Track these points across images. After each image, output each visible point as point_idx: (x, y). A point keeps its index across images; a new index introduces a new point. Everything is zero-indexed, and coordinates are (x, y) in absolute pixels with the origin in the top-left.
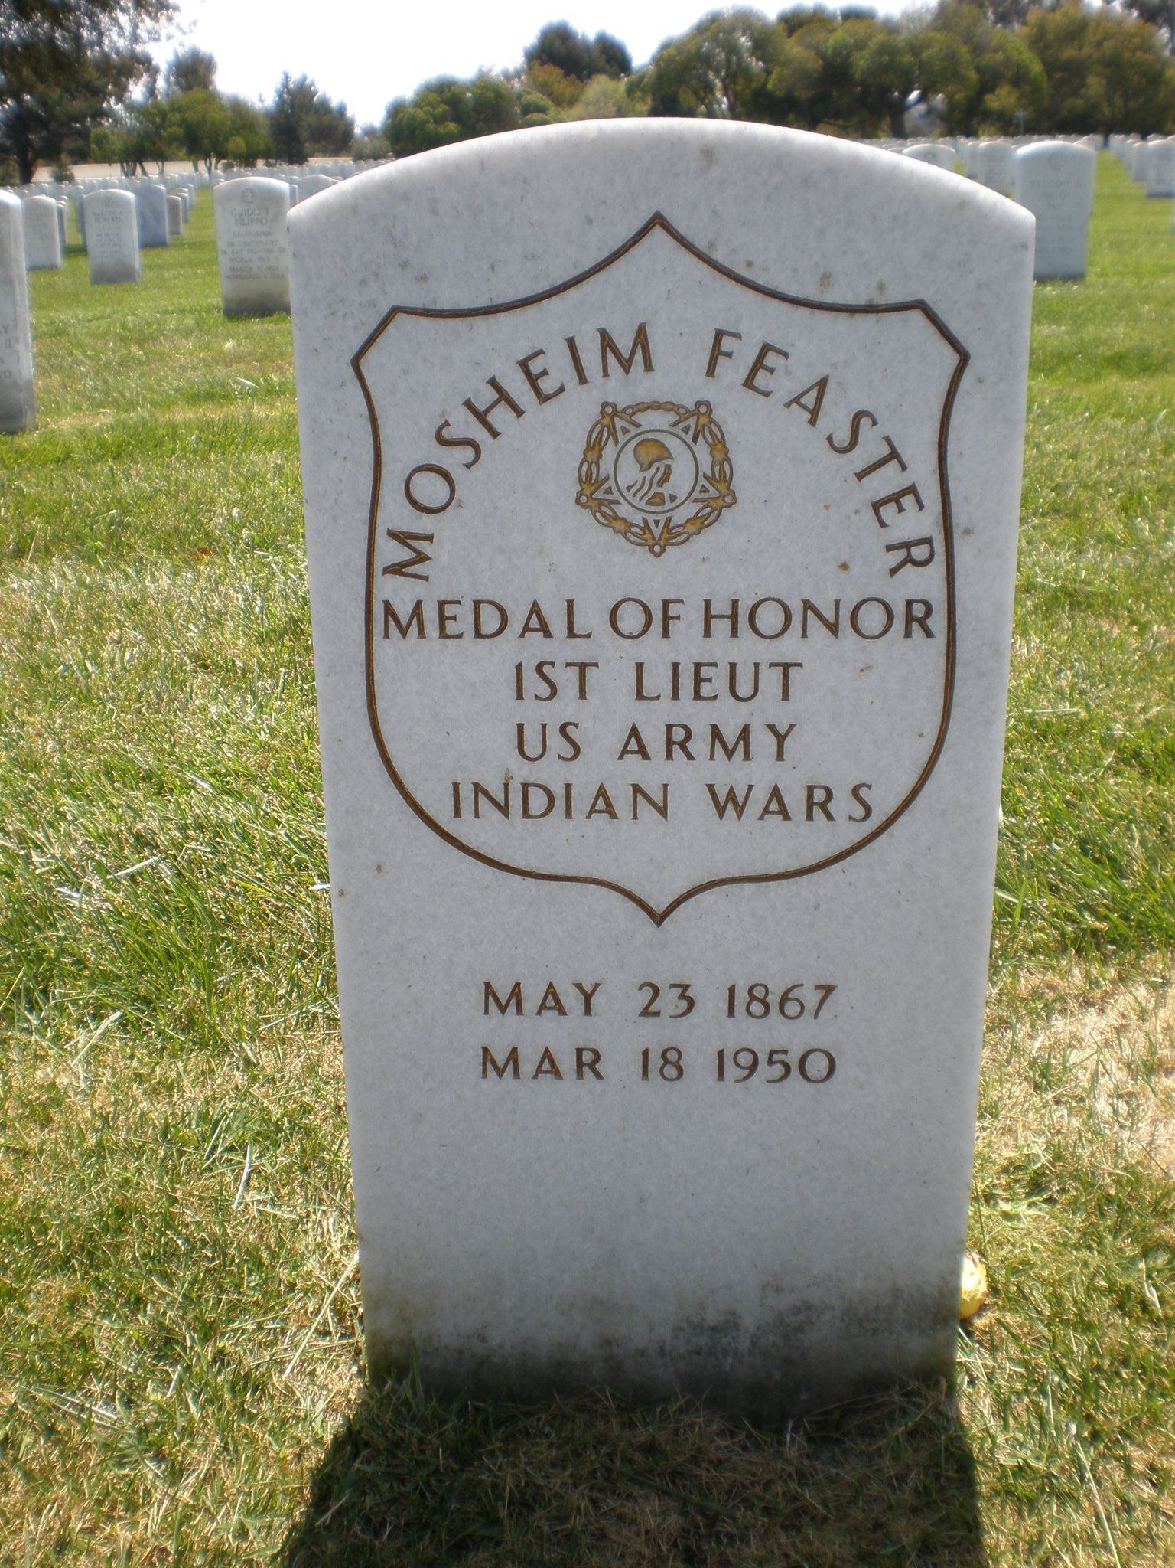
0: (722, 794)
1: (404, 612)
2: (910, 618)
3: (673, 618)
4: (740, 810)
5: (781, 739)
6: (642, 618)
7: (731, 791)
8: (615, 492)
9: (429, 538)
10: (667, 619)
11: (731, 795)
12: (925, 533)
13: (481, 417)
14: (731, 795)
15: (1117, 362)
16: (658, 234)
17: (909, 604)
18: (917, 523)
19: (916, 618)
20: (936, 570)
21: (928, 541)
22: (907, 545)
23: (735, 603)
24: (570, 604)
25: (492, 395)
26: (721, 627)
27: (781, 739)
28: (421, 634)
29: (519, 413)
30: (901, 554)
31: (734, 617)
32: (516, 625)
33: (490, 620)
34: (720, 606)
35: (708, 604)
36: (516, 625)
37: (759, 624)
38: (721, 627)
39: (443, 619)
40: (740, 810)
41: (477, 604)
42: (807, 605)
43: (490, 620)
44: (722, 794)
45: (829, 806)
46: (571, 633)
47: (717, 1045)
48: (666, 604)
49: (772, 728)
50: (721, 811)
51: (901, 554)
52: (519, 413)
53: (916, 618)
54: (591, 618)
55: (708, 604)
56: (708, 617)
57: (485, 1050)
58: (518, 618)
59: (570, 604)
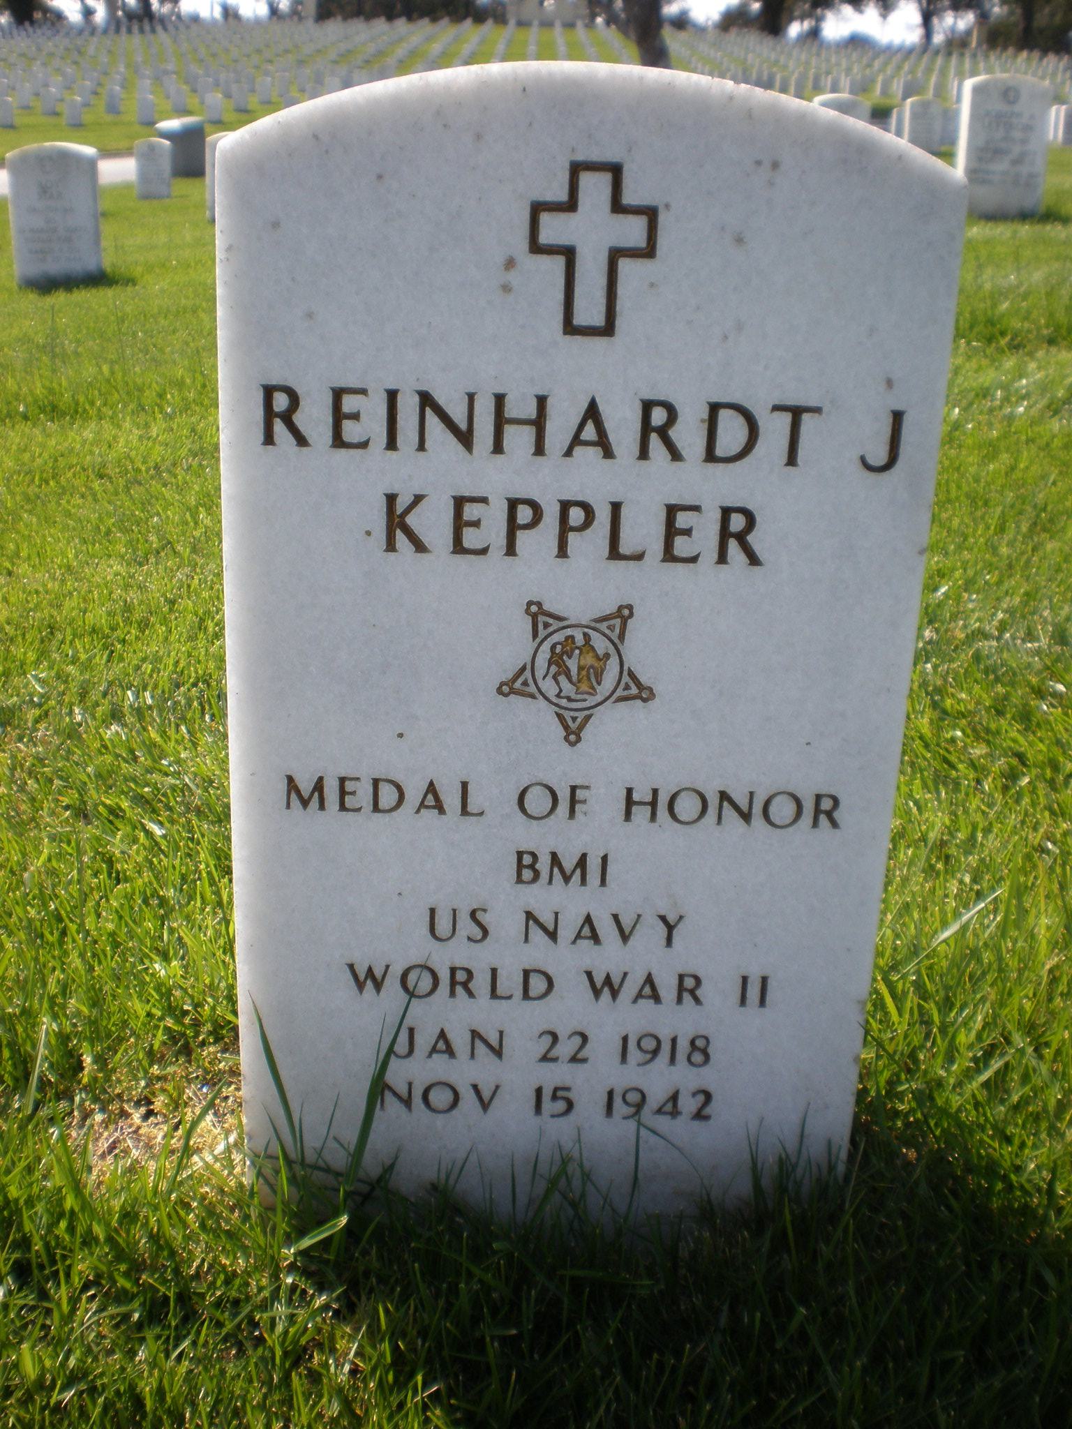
0: (599, 979)
2: (817, 811)
4: (615, 994)
5: (670, 928)
7: (608, 977)
10: (573, 801)
11: (608, 981)
13: (500, 421)
14: (608, 981)
15: (385, 795)
17: (818, 798)
24: (465, 785)
25: (531, 411)
26: (641, 814)
27: (670, 928)
28: (322, 806)
29: (539, 450)
31: (653, 804)
33: (388, 796)
35: (629, 791)
37: (677, 810)
38: (641, 814)
39: (343, 793)
40: (615, 994)
41: (376, 782)
42: (724, 796)
43: (388, 796)
44: (599, 979)
45: (836, 815)
46: (465, 811)
48: (573, 789)
49: (663, 919)
52: (539, 450)
55: (629, 791)
56: (630, 802)
57: (290, 779)
58: (414, 794)
59: (465, 785)
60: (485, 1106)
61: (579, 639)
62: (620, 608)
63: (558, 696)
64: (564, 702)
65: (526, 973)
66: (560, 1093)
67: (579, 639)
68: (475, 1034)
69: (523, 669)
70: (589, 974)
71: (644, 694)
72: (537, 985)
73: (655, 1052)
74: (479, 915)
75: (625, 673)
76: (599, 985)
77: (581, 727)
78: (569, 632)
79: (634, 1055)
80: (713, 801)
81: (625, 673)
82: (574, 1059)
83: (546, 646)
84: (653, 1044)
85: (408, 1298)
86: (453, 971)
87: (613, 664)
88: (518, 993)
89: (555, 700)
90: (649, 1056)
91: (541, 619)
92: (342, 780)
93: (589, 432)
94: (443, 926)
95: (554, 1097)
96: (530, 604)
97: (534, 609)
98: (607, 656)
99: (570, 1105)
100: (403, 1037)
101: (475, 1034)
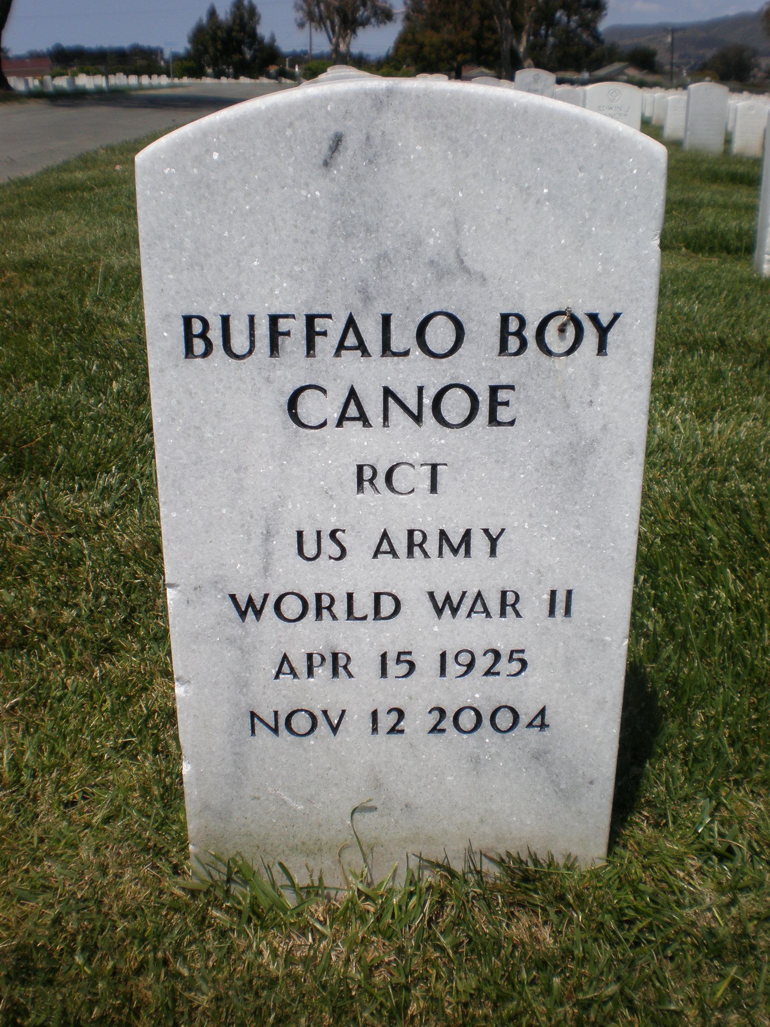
0: (440, 600)
4: (455, 611)
44: (440, 600)
60: (335, 729)
65: (377, 596)
66: (403, 658)
68: (388, 393)
70: (431, 595)
72: (387, 606)
74: (339, 535)
79: (453, 669)
82: (393, 730)
86: (318, 596)
88: (371, 616)
90: (465, 668)
93: (353, 411)
94: (310, 549)
95: (398, 661)
99: (412, 665)
101: (388, 393)
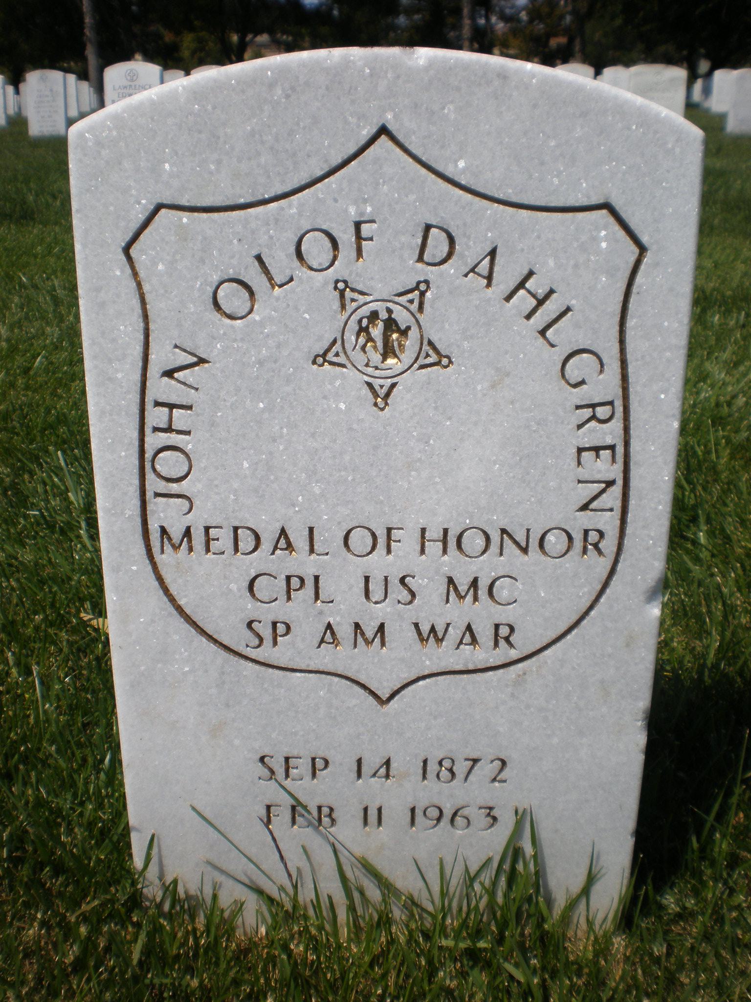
0: (425, 628)
1: (176, 533)
3: (534, 296)
4: (439, 641)
6: (369, 541)
8: (354, 305)
9: (191, 549)
12: (609, 441)
16: (383, 137)
18: (604, 387)
19: (591, 542)
20: (617, 425)
21: (611, 403)
22: (593, 406)
23: (446, 531)
26: (433, 548)
30: (588, 413)
31: (445, 541)
32: (266, 545)
33: (246, 541)
34: (434, 533)
35: (423, 530)
36: (266, 545)
38: (433, 548)
41: (236, 529)
44: (425, 628)
47: (410, 802)
50: (423, 640)
51: (588, 413)
53: (591, 542)
54: (329, 537)
55: (423, 530)
61: (384, 315)
62: (419, 283)
63: (367, 365)
64: (370, 370)
67: (384, 315)
69: (334, 342)
71: (442, 360)
73: (439, 819)
75: (425, 342)
76: (425, 635)
77: (388, 395)
78: (373, 306)
80: (495, 537)
81: (425, 342)
83: (355, 317)
84: (436, 813)
85: (72, 829)
87: (414, 333)
89: (364, 369)
91: (348, 294)
92: (207, 529)
96: (337, 282)
97: (341, 285)
98: (408, 328)
100: (356, 895)
